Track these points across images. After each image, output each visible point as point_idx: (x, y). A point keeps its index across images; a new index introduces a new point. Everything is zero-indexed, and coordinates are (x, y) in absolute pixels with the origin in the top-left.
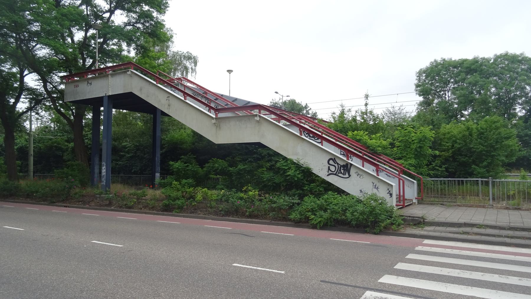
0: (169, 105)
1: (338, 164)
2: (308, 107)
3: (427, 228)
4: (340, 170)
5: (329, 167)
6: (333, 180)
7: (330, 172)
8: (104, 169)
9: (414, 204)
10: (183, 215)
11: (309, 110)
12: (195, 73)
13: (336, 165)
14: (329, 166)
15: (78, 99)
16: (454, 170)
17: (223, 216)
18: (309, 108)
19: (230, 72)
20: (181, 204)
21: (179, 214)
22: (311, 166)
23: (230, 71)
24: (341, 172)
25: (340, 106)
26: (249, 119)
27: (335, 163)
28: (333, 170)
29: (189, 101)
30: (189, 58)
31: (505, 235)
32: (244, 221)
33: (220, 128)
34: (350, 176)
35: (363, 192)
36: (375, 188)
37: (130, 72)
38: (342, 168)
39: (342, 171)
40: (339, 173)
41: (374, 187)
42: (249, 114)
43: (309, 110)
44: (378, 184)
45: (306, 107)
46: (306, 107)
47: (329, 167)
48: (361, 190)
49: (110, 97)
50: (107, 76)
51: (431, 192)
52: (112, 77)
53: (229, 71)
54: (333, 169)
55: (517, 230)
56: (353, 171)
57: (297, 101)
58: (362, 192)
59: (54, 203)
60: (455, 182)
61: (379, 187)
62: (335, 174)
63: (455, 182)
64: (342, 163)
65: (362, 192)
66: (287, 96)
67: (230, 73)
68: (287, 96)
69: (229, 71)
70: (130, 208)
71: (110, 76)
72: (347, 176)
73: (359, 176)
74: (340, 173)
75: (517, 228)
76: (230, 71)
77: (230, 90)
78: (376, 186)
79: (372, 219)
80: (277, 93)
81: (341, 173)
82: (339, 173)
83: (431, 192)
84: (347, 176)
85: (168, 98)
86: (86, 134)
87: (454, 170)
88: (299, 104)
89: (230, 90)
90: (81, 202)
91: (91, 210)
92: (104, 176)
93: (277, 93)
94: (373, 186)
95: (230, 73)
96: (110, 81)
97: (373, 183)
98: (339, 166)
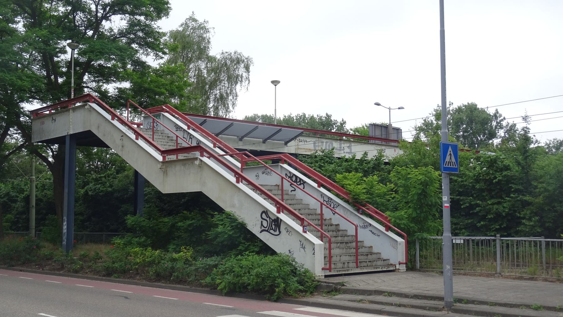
0: (123, 146)
1: (270, 218)
2: (501, 116)
3: (339, 296)
4: (272, 226)
5: (262, 222)
6: (265, 237)
7: (263, 228)
8: (65, 225)
9: (397, 270)
10: (118, 281)
11: (502, 120)
12: (247, 82)
13: (268, 219)
14: (262, 220)
15: (43, 140)
16: (551, 225)
17: (104, 276)
18: (502, 118)
19: (275, 84)
20: (119, 267)
21: (118, 279)
22: (246, 221)
23: (275, 83)
24: (272, 228)
25: (412, 129)
26: (192, 162)
27: (268, 218)
28: (266, 226)
29: (141, 142)
30: (238, 61)
31: (395, 303)
32: (169, 287)
33: (167, 174)
34: (280, 232)
35: (292, 252)
36: (302, 247)
37: (88, 106)
38: (273, 223)
39: (273, 227)
40: (270, 229)
41: (301, 246)
42: (239, 152)
43: (502, 120)
44: (305, 243)
45: (496, 116)
46: (496, 116)
47: (262, 222)
48: (290, 251)
49: (72, 136)
50: (69, 110)
51: (487, 257)
52: (74, 112)
53: (273, 82)
54: (265, 224)
55: (419, 299)
56: (282, 227)
57: (479, 106)
58: (291, 253)
59: (13, 266)
60: (530, 244)
61: (305, 247)
62: (267, 231)
63: (530, 244)
64: (273, 218)
65: (291, 253)
66: (399, 108)
67: (276, 85)
68: (399, 108)
69: (273, 82)
70: (76, 272)
71: (71, 111)
72: (277, 233)
73: (288, 232)
74: (271, 229)
75: (420, 296)
76: (275, 83)
77: (275, 110)
78: (303, 244)
79: (269, 283)
80: (378, 104)
81: (272, 229)
82: (270, 229)
83: (487, 257)
84: (277, 233)
85: (122, 137)
86: (100, 177)
87: (551, 225)
88: (483, 111)
89: (275, 110)
90: (38, 265)
91: (61, 277)
92: (64, 233)
93: (378, 104)
94: (301, 245)
95: (276, 85)
96: (71, 117)
97: (301, 242)
98: (271, 220)
